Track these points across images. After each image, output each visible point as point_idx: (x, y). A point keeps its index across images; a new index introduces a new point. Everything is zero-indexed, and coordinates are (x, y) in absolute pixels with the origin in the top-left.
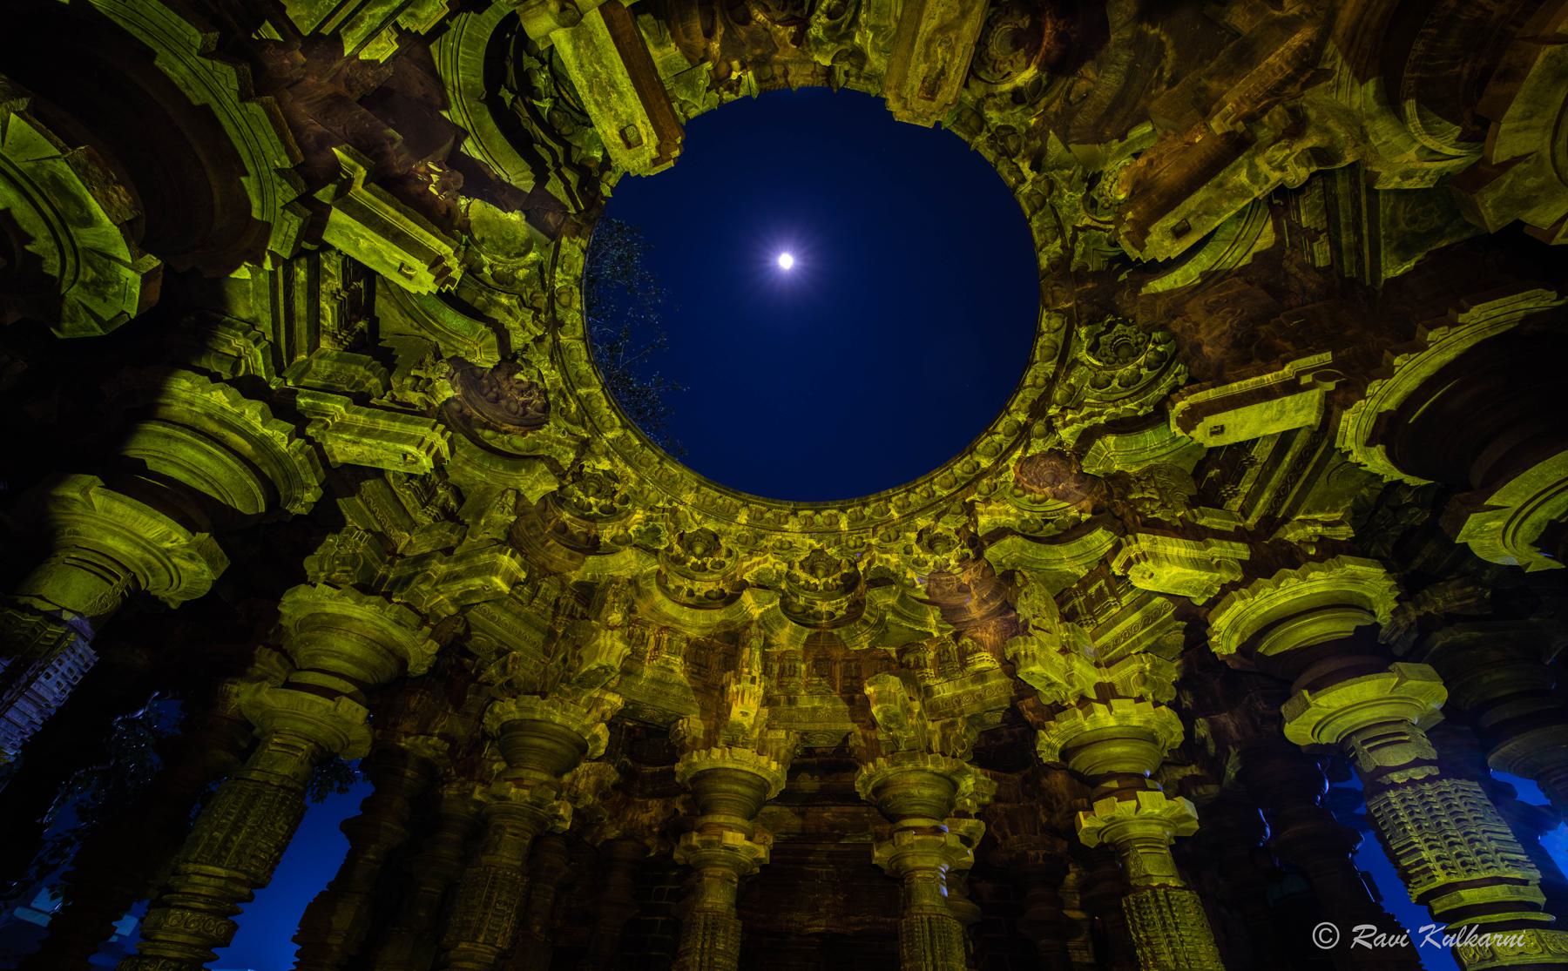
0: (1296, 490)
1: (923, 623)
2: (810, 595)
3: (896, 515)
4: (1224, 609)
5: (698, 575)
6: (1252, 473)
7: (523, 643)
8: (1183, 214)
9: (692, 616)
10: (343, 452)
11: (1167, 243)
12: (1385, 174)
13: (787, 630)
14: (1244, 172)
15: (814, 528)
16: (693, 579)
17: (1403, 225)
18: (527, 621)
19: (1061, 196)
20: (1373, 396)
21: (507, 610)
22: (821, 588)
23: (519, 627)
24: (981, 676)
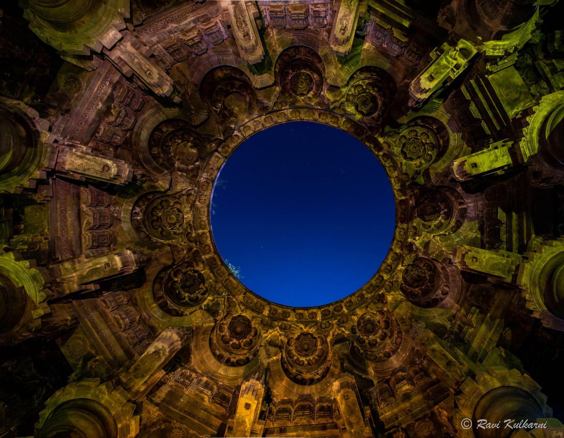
0: (525, 225)
1: (365, 372)
2: (300, 368)
3: (346, 311)
4: (522, 272)
5: (235, 351)
6: (503, 228)
7: (107, 352)
8: (430, 73)
9: (226, 371)
10: (72, 163)
11: (428, 83)
12: (487, 49)
13: (284, 383)
14: (444, 60)
15: (303, 320)
16: (231, 353)
17: (505, 97)
18: (119, 339)
19: (393, 149)
20: (527, 134)
21: (109, 327)
22: (306, 362)
23: (112, 340)
24: (407, 397)
